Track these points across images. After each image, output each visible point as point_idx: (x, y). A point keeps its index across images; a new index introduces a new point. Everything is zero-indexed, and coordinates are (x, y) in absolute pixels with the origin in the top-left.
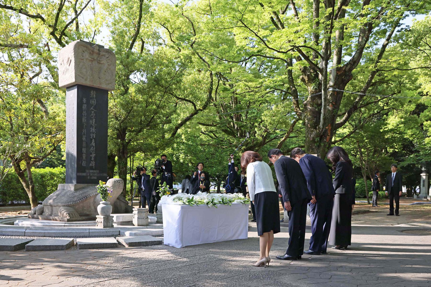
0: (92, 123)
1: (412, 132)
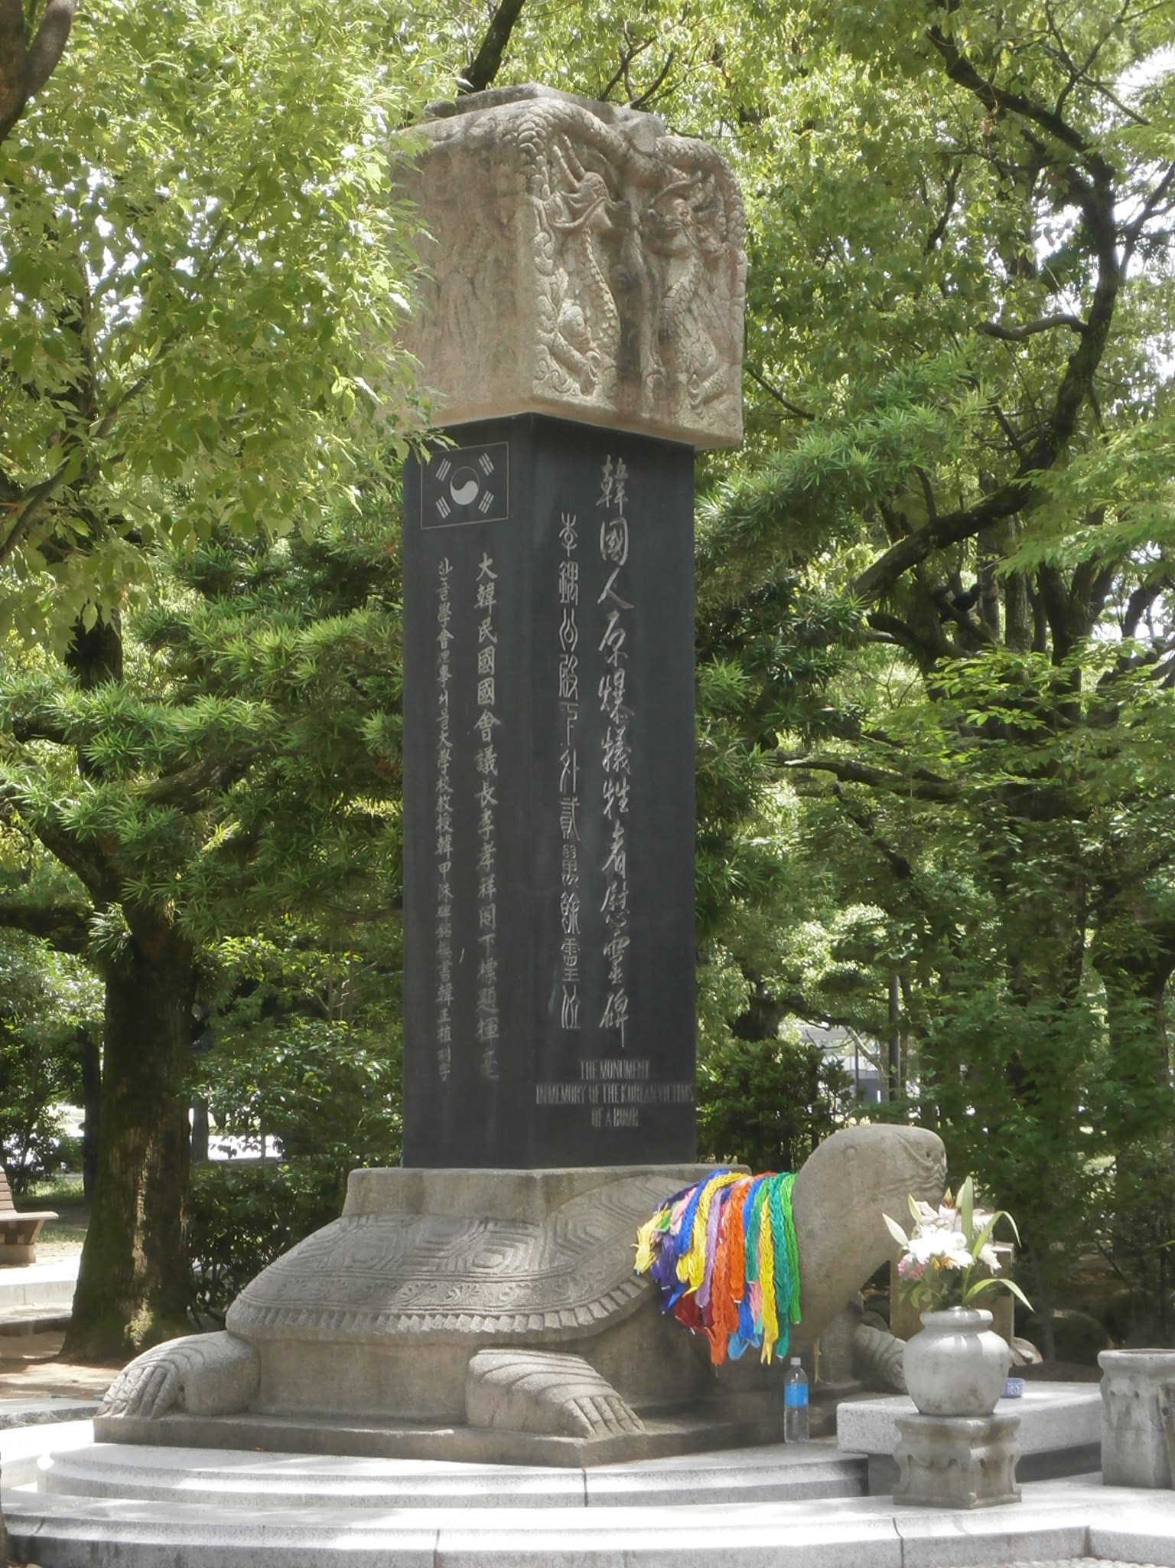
0: (611, 700)
1: (1162, 168)
